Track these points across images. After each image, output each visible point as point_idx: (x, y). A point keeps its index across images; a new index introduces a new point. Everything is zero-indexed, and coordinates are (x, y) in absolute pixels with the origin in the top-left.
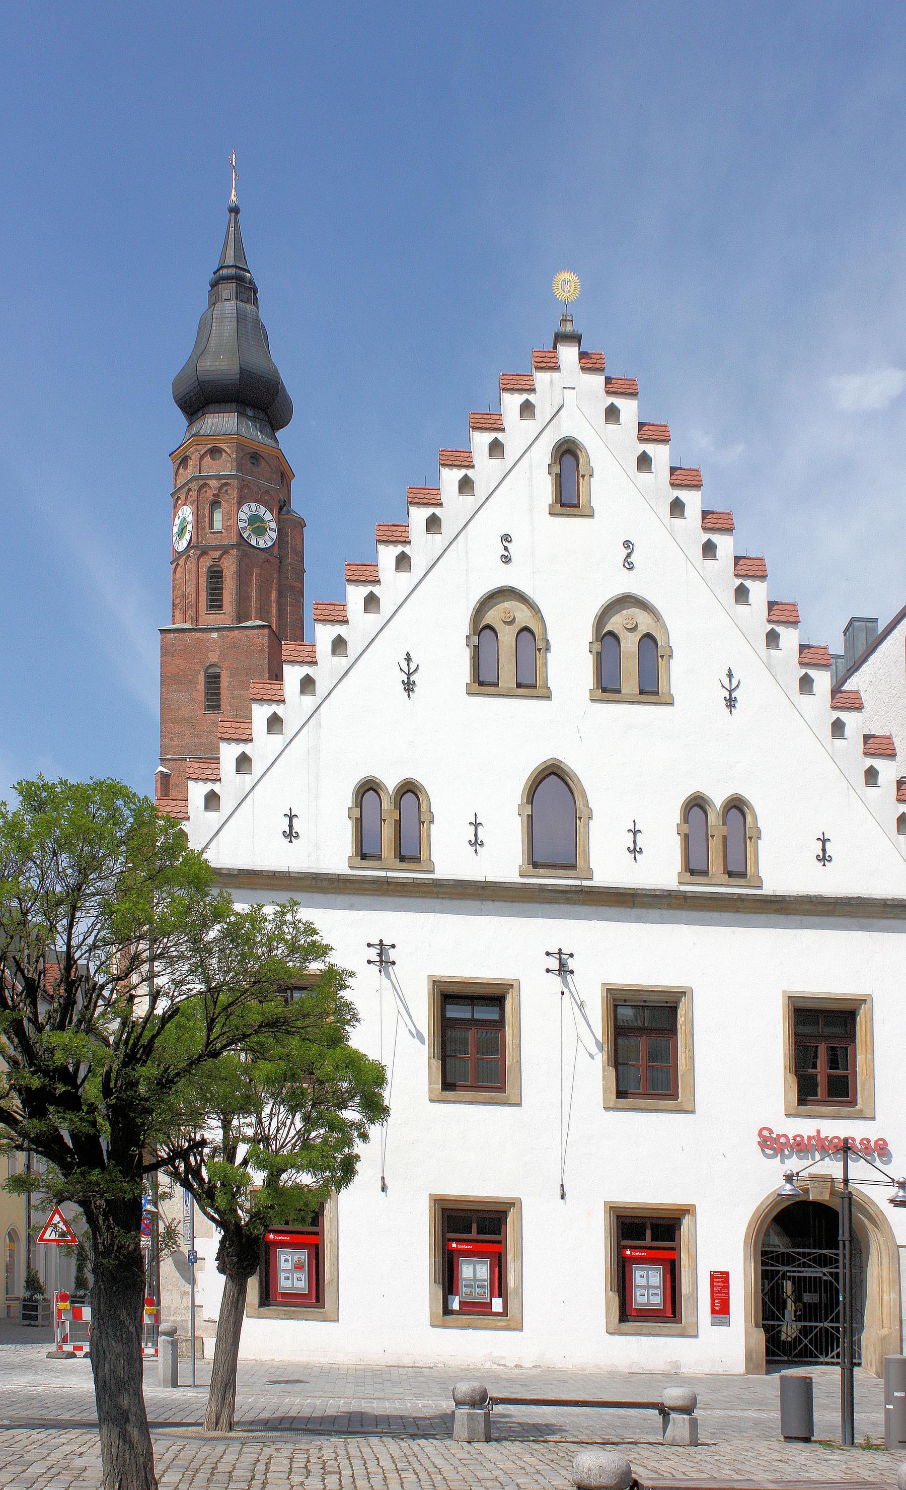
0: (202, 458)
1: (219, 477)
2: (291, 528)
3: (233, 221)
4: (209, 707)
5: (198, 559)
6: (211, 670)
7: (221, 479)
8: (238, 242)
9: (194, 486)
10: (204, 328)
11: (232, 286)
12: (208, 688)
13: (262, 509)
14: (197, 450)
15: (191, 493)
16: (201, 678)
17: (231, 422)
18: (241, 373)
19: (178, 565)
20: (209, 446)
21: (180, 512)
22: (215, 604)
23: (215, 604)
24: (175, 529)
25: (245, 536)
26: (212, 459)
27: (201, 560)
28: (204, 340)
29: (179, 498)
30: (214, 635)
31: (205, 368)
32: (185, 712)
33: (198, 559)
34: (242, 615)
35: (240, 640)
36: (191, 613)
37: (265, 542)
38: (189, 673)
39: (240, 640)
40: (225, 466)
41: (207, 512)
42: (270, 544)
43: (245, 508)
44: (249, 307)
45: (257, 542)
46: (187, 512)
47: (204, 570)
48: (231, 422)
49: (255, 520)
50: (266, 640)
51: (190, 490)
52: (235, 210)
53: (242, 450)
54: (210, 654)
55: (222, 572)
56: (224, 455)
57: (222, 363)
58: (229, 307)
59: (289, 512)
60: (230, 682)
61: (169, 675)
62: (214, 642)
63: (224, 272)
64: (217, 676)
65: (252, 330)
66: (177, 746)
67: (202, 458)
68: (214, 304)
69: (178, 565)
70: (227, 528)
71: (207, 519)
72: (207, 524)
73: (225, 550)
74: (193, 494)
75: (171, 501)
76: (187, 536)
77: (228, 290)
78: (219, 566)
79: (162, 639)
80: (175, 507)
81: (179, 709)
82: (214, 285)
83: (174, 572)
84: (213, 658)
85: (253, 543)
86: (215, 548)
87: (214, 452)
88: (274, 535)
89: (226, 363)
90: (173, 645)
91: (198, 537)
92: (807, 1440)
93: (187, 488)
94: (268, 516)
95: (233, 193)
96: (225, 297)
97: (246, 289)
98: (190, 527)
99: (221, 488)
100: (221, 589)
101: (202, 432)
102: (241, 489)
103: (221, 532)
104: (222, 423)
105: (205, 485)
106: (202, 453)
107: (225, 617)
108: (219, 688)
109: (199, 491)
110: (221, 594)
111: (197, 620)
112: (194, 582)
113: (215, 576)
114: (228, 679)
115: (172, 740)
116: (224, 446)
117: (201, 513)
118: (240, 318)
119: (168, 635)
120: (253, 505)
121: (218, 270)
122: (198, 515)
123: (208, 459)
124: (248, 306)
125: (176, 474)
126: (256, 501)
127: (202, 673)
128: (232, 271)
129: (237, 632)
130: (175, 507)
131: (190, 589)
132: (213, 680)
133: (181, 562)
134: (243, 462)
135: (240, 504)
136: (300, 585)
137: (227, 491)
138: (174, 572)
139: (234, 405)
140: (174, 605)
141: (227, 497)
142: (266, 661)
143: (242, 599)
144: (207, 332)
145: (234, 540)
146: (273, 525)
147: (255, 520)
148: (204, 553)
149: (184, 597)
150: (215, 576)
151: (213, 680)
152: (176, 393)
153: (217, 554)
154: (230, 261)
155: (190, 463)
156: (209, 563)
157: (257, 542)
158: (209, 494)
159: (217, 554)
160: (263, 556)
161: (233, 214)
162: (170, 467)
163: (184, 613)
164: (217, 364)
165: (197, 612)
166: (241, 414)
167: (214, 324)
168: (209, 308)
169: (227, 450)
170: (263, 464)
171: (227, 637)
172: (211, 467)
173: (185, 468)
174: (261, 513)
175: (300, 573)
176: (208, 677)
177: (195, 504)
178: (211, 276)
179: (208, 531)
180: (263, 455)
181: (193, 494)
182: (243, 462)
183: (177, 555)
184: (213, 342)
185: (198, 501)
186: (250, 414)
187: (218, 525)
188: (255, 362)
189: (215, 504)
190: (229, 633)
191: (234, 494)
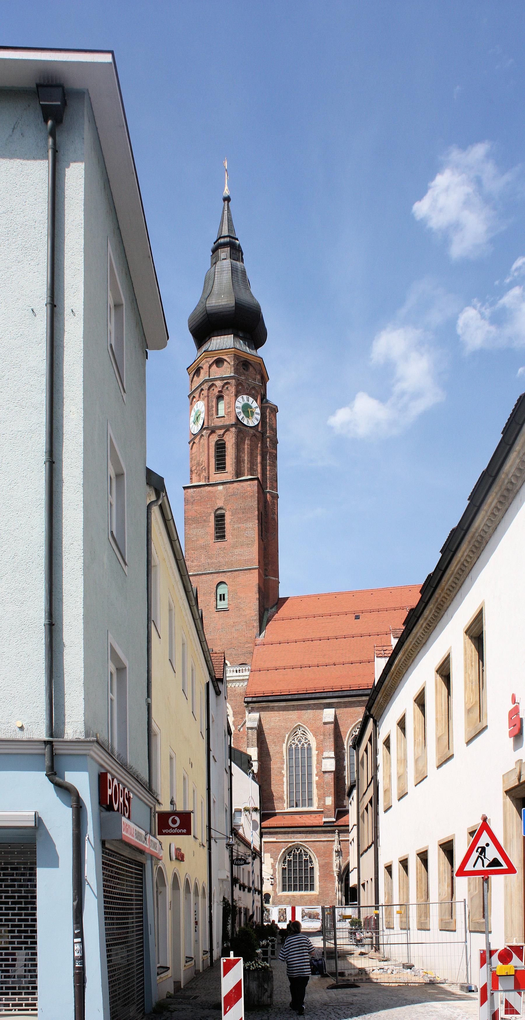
0: (210, 366)
1: (222, 379)
2: (269, 411)
3: (226, 207)
4: (218, 538)
5: (209, 437)
6: (219, 512)
7: (223, 380)
8: (230, 220)
9: (205, 387)
10: (209, 281)
11: (228, 249)
12: (217, 525)
13: (251, 399)
14: (207, 362)
15: (203, 392)
16: (212, 518)
17: (229, 341)
18: (236, 303)
19: (194, 443)
20: (215, 358)
21: (195, 407)
22: (221, 466)
23: (221, 466)
24: (192, 419)
25: (240, 418)
26: (217, 367)
27: (211, 437)
28: (210, 287)
29: (194, 397)
30: (220, 488)
31: (212, 305)
32: (201, 542)
33: (209, 437)
34: (238, 473)
35: (238, 489)
36: (204, 474)
37: (253, 422)
38: (203, 515)
39: (238, 489)
40: (227, 370)
41: (214, 404)
42: (256, 423)
43: (240, 398)
44: (239, 264)
45: (248, 422)
46: (200, 406)
47: (212, 444)
48: (229, 341)
49: (246, 409)
50: (256, 488)
51: (202, 390)
52: (227, 199)
53: (238, 359)
54: (218, 501)
55: (225, 444)
56: (225, 363)
57: (222, 300)
58: (225, 264)
59: (267, 401)
60: (231, 519)
61: (190, 517)
62: (221, 492)
63: (222, 241)
64: (223, 516)
65: (239, 277)
66: (196, 566)
67: (210, 366)
68: (216, 263)
69: (194, 443)
70: (228, 414)
71: (214, 409)
72: (214, 412)
73: (227, 428)
74: (205, 392)
75: (188, 401)
76: (201, 422)
77: (224, 253)
78: (223, 440)
79: (185, 494)
80: (191, 404)
81: (197, 540)
82: (214, 251)
83: (192, 449)
84: (220, 504)
85: (245, 423)
86: (220, 428)
87: (219, 362)
88: (259, 417)
89: (226, 300)
90: (193, 497)
91: (208, 422)
92: (232, 862)
93: (200, 389)
94: (254, 405)
95: (226, 188)
96: (222, 257)
97: (236, 252)
98: (202, 416)
99: (223, 387)
100: (225, 455)
101: (210, 349)
102: (237, 386)
103: (224, 417)
104: (223, 342)
105: (213, 385)
106: (210, 363)
107: (229, 474)
108: (224, 524)
109: (209, 389)
110: (225, 459)
111: (209, 479)
112: (206, 452)
113: (220, 447)
114: (231, 517)
115: (192, 561)
116: (225, 357)
117: (210, 405)
118: (234, 270)
119: (189, 490)
120: (245, 397)
121: (217, 240)
122: (208, 406)
123: (214, 366)
124: (238, 263)
125: (192, 382)
126: (247, 394)
127: (213, 515)
128: (227, 239)
129: (235, 484)
130: (191, 404)
131: (204, 458)
132: (220, 519)
133: (197, 441)
134: (238, 367)
135: (237, 396)
136: (275, 452)
137: (227, 388)
138: (192, 449)
139: (231, 331)
140: (191, 471)
141: (227, 392)
142: (256, 503)
143: (239, 461)
144: (211, 282)
145: (233, 421)
146: (258, 410)
147: (246, 409)
148: (213, 432)
149: (198, 464)
150: (220, 447)
151: (220, 519)
152: (191, 326)
153: (222, 432)
154: (225, 232)
155: (202, 371)
156: (216, 438)
157: (256, 407)
158: (216, 391)
159: (222, 432)
160: (252, 431)
161: (226, 202)
162: (188, 378)
163: (199, 475)
164: (220, 301)
165: (209, 472)
166: (236, 336)
167: (216, 276)
168: (212, 266)
169: (227, 359)
170: (251, 369)
171: (229, 488)
172: (216, 372)
173: (198, 376)
174: (250, 403)
175: (275, 443)
176: (216, 517)
177: (206, 398)
178: (212, 246)
179: (215, 416)
180: (251, 362)
181: (205, 392)
182: (238, 367)
183: (193, 437)
184: (216, 288)
185: (208, 396)
186: (241, 335)
187: (221, 413)
188: (244, 297)
189: (220, 397)
190: (231, 485)
191: (232, 389)
